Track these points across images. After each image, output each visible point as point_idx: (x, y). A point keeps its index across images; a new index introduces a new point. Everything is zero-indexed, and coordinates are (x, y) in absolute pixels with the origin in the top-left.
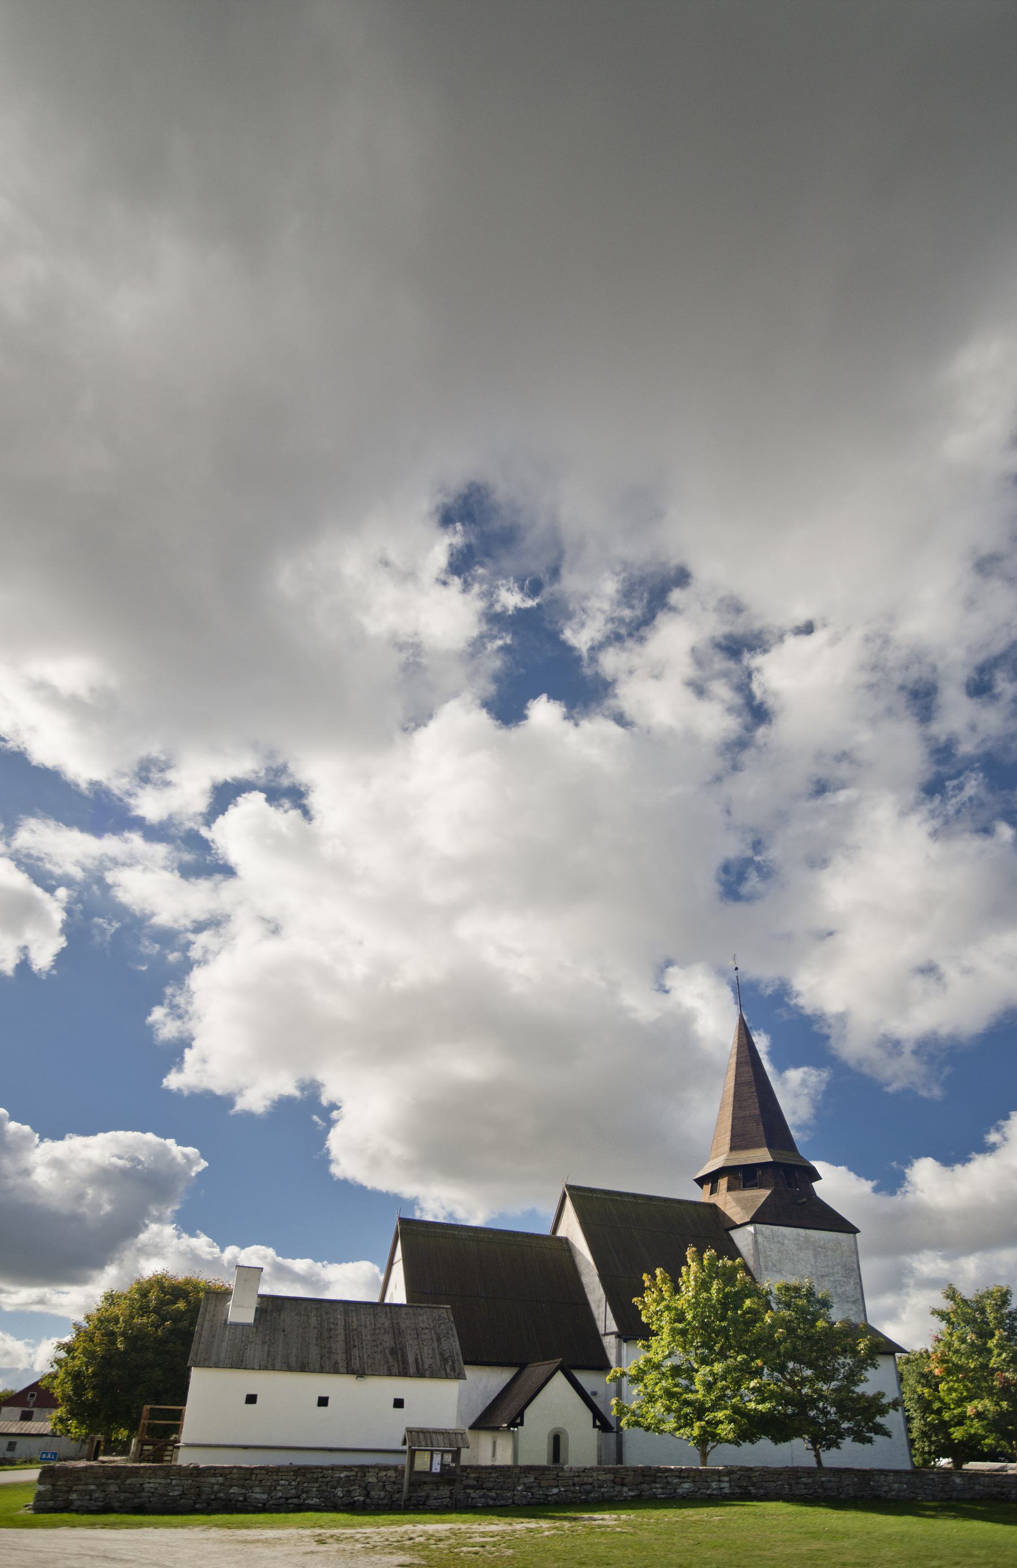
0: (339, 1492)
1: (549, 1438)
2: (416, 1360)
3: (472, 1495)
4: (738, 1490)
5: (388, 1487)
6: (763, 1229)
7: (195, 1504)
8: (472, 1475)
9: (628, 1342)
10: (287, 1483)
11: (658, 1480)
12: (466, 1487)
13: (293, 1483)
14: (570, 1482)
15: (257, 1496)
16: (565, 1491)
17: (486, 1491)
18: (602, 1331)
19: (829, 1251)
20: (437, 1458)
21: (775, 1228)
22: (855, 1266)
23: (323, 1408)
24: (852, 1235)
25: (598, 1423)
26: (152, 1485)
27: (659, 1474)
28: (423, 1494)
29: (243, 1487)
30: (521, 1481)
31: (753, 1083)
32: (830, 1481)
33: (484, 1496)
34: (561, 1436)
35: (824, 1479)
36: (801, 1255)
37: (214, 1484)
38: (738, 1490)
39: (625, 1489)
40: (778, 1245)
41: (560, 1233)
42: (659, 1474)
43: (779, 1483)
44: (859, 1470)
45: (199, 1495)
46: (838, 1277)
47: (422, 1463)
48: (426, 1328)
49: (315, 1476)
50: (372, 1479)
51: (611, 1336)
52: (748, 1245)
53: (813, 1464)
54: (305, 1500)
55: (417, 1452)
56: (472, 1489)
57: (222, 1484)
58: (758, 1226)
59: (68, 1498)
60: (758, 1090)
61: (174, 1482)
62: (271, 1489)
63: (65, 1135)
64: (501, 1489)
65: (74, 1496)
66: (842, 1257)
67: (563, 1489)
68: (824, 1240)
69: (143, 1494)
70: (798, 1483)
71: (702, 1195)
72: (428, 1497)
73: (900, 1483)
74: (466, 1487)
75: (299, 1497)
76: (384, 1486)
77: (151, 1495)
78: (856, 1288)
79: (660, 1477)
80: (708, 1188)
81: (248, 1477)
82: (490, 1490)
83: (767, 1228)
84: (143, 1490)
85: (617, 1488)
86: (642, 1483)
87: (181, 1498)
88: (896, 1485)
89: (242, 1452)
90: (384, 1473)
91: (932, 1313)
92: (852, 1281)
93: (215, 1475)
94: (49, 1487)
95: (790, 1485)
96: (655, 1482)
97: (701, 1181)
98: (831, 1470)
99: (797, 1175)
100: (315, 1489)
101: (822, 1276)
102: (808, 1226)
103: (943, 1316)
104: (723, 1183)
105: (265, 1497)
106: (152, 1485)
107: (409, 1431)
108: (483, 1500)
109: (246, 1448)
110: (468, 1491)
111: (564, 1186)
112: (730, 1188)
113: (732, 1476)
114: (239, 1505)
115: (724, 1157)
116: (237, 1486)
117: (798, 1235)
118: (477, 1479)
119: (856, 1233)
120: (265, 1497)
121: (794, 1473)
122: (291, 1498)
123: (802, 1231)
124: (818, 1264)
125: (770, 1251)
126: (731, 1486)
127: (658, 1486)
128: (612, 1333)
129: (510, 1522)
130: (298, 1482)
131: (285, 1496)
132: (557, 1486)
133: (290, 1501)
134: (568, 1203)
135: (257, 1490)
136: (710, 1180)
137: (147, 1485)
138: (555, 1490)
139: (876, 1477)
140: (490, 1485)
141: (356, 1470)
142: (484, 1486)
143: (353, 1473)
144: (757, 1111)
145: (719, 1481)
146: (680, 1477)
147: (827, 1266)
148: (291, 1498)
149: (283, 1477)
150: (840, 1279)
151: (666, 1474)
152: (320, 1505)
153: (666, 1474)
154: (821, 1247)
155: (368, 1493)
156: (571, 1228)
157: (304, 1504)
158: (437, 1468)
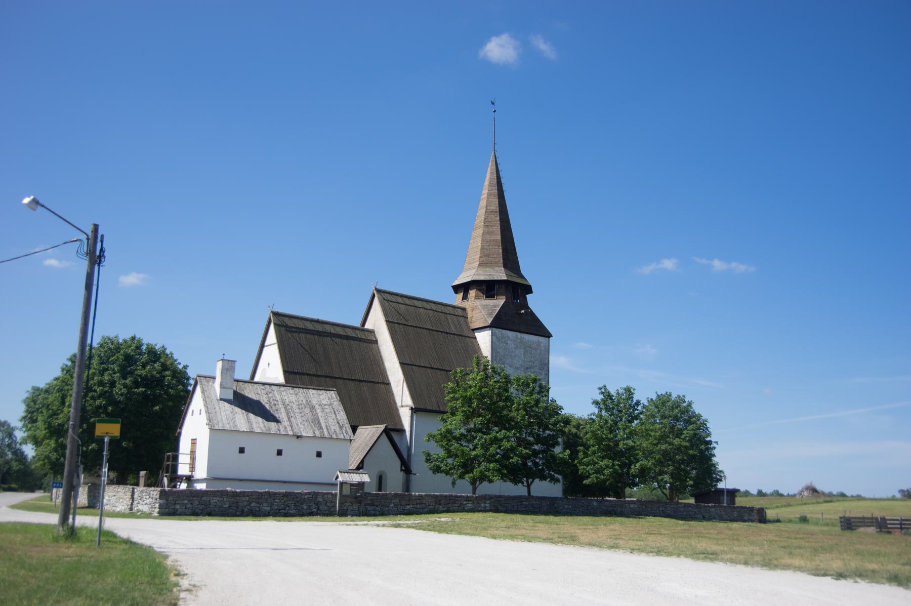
2: (327, 426)
3: (369, 509)
5: (328, 504)
6: (497, 332)
7: (236, 511)
8: (369, 498)
10: (279, 501)
14: (415, 502)
15: (266, 508)
16: (413, 507)
17: (375, 507)
18: (399, 404)
19: (533, 350)
22: (547, 362)
24: (547, 338)
25: (403, 468)
27: (457, 499)
29: (258, 503)
31: (498, 213)
33: (374, 510)
34: (383, 476)
35: (534, 502)
39: (441, 507)
42: (457, 499)
43: (513, 504)
45: (238, 507)
48: (326, 405)
49: (293, 497)
50: (321, 500)
51: (405, 408)
53: (526, 494)
55: (344, 484)
57: (248, 501)
58: (494, 329)
61: (225, 500)
62: (271, 505)
65: (178, 507)
66: (540, 355)
67: (412, 506)
68: (531, 341)
70: (521, 505)
71: (456, 300)
72: (347, 510)
73: (568, 505)
75: (285, 509)
76: (326, 503)
77: (205, 507)
78: (545, 377)
79: (457, 500)
80: (461, 295)
82: (377, 506)
83: (499, 331)
84: (210, 504)
85: (437, 506)
86: (449, 503)
87: (229, 509)
88: (566, 506)
90: (327, 496)
91: (593, 403)
94: (165, 501)
95: (518, 506)
96: (455, 503)
97: (457, 289)
99: (519, 290)
100: (293, 505)
101: (527, 368)
102: (523, 331)
103: (596, 403)
105: (269, 508)
110: (367, 507)
115: (474, 271)
119: (550, 337)
120: (269, 508)
121: (519, 498)
126: (490, 506)
127: (456, 505)
128: (407, 406)
129: (408, 519)
130: (285, 501)
132: (409, 505)
133: (281, 511)
134: (376, 302)
136: (463, 289)
137: (212, 501)
138: (408, 507)
141: (312, 494)
142: (375, 504)
143: (311, 496)
144: (499, 237)
146: (466, 501)
147: (531, 361)
148: (282, 509)
149: (277, 498)
151: (460, 499)
152: (296, 514)
153: (460, 499)
154: (529, 347)
156: (377, 322)
157: (288, 513)
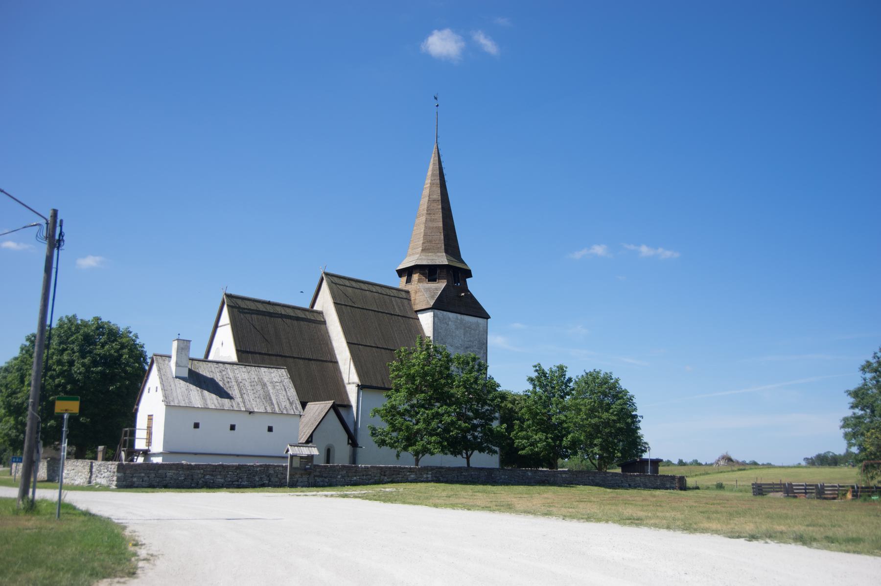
1: (325, 450)
2: (277, 402)
3: (318, 480)
4: (435, 479)
5: (279, 476)
7: (192, 484)
8: (318, 470)
9: (363, 389)
11: (400, 473)
12: (315, 476)
13: (235, 473)
18: (346, 381)
22: (485, 341)
23: (232, 431)
24: (486, 320)
25: (350, 442)
26: (170, 474)
28: (295, 480)
29: (212, 475)
30: (340, 473)
31: (440, 201)
32: (475, 474)
35: (472, 473)
36: (458, 332)
37: (198, 474)
38: (435, 479)
39: (386, 478)
40: (446, 325)
41: (317, 307)
44: (488, 469)
45: (193, 480)
52: (429, 324)
54: (241, 482)
56: (317, 477)
59: (132, 481)
60: (443, 208)
64: (331, 477)
65: (135, 479)
68: (470, 322)
69: (167, 479)
70: (461, 475)
71: (401, 283)
72: (297, 481)
74: (315, 476)
75: (238, 481)
76: (277, 475)
80: (404, 279)
81: (214, 470)
82: (325, 478)
84: (166, 477)
85: (382, 477)
87: (185, 481)
88: (503, 476)
89: (194, 456)
92: (482, 352)
93: (199, 469)
96: (399, 474)
97: (401, 273)
98: (476, 468)
100: (245, 477)
101: (467, 348)
103: (531, 380)
104: (416, 277)
105: (223, 480)
106: (170, 474)
108: (322, 483)
109: (196, 454)
110: (316, 478)
111: (322, 272)
112: (420, 281)
113: (433, 471)
114: (211, 485)
116: (209, 475)
117: (457, 318)
118: (320, 472)
120: (223, 480)
121: (459, 469)
122: (234, 481)
123: (459, 316)
124: (465, 339)
125: (441, 329)
127: (400, 476)
128: (353, 383)
131: (232, 480)
132: (355, 476)
133: (234, 483)
134: (325, 285)
135: (219, 477)
136: (407, 273)
137: (168, 474)
138: (355, 478)
139: (495, 472)
140: (326, 475)
143: (263, 468)
144: (441, 224)
145: (427, 474)
146: (409, 472)
148: (234, 481)
150: (476, 349)
153: (404, 470)
155: (270, 479)
156: (326, 304)
157: (241, 485)
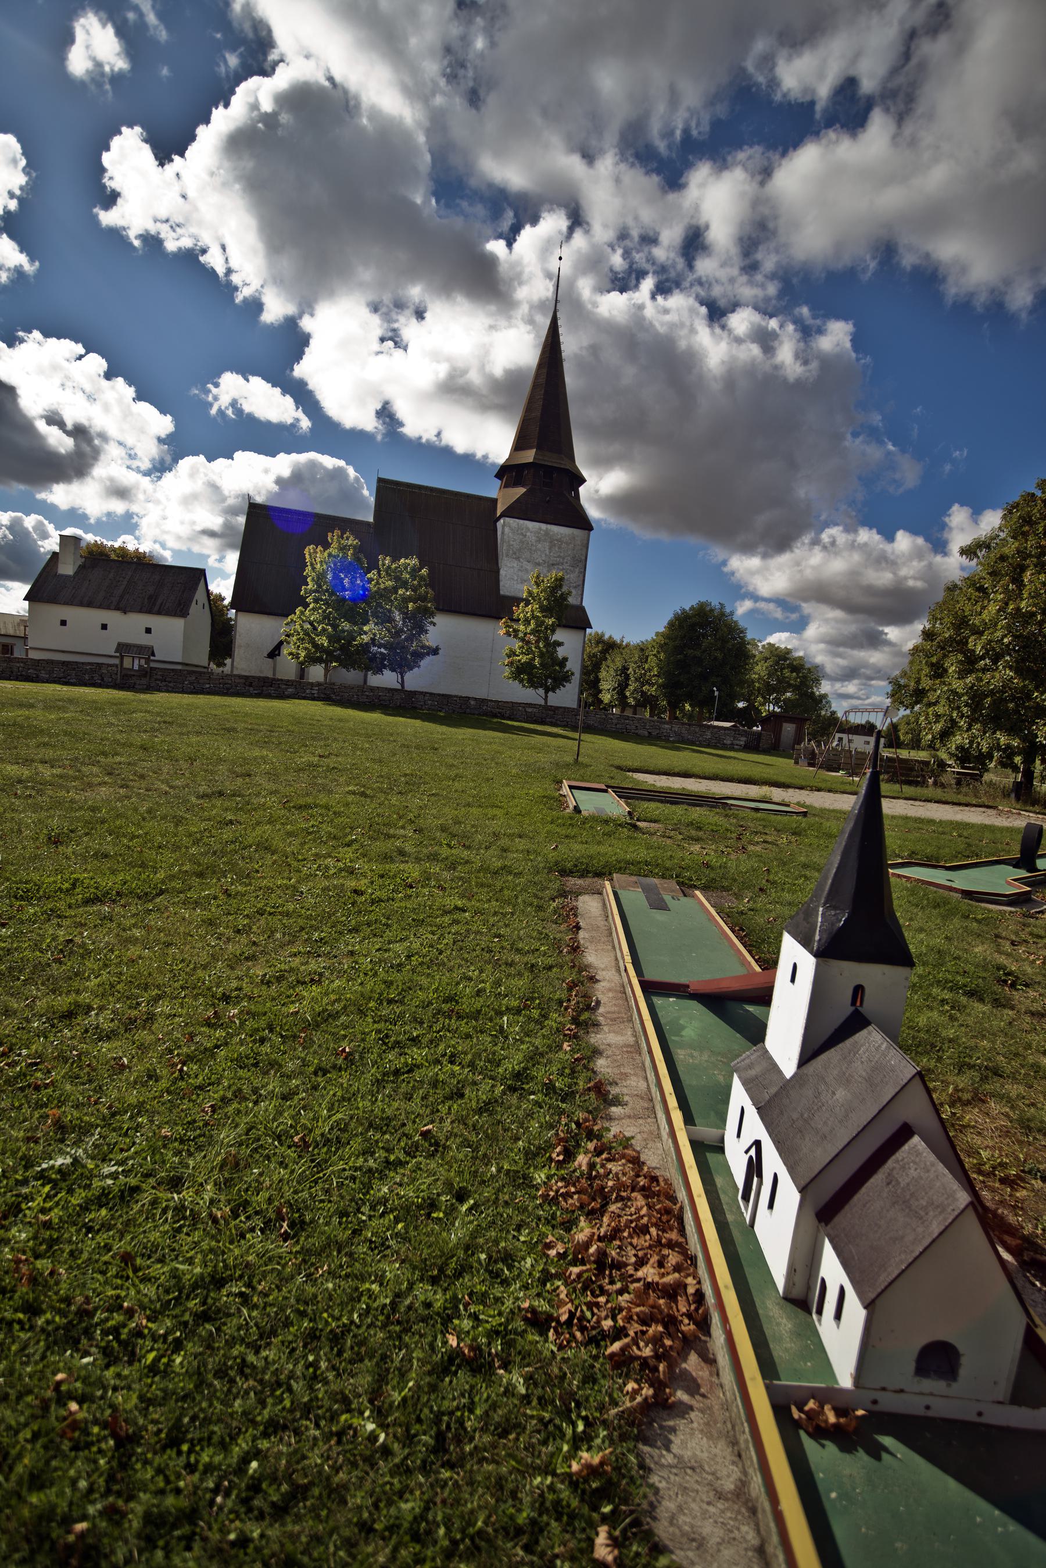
0: (87, 677)
20: (136, 662)
21: (521, 522)
46: (566, 566)
47: (127, 663)
63: (176, 426)
107: (119, 644)
123: (544, 526)
158: (136, 667)
